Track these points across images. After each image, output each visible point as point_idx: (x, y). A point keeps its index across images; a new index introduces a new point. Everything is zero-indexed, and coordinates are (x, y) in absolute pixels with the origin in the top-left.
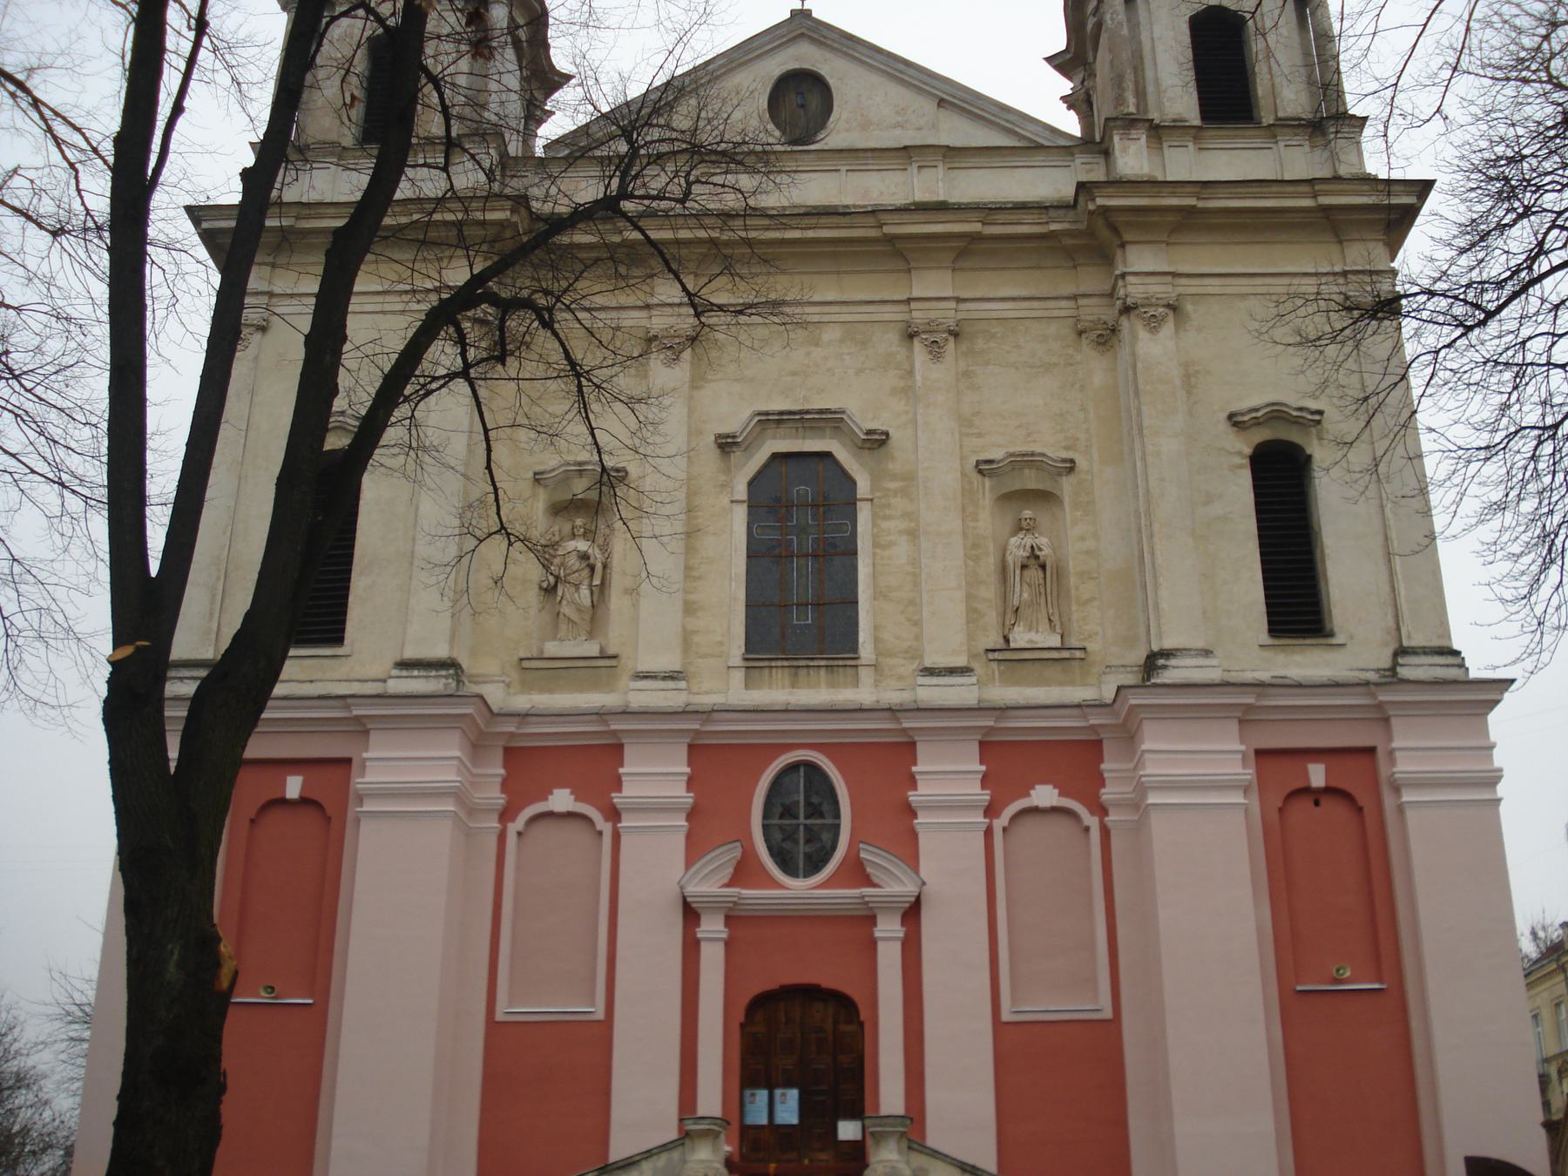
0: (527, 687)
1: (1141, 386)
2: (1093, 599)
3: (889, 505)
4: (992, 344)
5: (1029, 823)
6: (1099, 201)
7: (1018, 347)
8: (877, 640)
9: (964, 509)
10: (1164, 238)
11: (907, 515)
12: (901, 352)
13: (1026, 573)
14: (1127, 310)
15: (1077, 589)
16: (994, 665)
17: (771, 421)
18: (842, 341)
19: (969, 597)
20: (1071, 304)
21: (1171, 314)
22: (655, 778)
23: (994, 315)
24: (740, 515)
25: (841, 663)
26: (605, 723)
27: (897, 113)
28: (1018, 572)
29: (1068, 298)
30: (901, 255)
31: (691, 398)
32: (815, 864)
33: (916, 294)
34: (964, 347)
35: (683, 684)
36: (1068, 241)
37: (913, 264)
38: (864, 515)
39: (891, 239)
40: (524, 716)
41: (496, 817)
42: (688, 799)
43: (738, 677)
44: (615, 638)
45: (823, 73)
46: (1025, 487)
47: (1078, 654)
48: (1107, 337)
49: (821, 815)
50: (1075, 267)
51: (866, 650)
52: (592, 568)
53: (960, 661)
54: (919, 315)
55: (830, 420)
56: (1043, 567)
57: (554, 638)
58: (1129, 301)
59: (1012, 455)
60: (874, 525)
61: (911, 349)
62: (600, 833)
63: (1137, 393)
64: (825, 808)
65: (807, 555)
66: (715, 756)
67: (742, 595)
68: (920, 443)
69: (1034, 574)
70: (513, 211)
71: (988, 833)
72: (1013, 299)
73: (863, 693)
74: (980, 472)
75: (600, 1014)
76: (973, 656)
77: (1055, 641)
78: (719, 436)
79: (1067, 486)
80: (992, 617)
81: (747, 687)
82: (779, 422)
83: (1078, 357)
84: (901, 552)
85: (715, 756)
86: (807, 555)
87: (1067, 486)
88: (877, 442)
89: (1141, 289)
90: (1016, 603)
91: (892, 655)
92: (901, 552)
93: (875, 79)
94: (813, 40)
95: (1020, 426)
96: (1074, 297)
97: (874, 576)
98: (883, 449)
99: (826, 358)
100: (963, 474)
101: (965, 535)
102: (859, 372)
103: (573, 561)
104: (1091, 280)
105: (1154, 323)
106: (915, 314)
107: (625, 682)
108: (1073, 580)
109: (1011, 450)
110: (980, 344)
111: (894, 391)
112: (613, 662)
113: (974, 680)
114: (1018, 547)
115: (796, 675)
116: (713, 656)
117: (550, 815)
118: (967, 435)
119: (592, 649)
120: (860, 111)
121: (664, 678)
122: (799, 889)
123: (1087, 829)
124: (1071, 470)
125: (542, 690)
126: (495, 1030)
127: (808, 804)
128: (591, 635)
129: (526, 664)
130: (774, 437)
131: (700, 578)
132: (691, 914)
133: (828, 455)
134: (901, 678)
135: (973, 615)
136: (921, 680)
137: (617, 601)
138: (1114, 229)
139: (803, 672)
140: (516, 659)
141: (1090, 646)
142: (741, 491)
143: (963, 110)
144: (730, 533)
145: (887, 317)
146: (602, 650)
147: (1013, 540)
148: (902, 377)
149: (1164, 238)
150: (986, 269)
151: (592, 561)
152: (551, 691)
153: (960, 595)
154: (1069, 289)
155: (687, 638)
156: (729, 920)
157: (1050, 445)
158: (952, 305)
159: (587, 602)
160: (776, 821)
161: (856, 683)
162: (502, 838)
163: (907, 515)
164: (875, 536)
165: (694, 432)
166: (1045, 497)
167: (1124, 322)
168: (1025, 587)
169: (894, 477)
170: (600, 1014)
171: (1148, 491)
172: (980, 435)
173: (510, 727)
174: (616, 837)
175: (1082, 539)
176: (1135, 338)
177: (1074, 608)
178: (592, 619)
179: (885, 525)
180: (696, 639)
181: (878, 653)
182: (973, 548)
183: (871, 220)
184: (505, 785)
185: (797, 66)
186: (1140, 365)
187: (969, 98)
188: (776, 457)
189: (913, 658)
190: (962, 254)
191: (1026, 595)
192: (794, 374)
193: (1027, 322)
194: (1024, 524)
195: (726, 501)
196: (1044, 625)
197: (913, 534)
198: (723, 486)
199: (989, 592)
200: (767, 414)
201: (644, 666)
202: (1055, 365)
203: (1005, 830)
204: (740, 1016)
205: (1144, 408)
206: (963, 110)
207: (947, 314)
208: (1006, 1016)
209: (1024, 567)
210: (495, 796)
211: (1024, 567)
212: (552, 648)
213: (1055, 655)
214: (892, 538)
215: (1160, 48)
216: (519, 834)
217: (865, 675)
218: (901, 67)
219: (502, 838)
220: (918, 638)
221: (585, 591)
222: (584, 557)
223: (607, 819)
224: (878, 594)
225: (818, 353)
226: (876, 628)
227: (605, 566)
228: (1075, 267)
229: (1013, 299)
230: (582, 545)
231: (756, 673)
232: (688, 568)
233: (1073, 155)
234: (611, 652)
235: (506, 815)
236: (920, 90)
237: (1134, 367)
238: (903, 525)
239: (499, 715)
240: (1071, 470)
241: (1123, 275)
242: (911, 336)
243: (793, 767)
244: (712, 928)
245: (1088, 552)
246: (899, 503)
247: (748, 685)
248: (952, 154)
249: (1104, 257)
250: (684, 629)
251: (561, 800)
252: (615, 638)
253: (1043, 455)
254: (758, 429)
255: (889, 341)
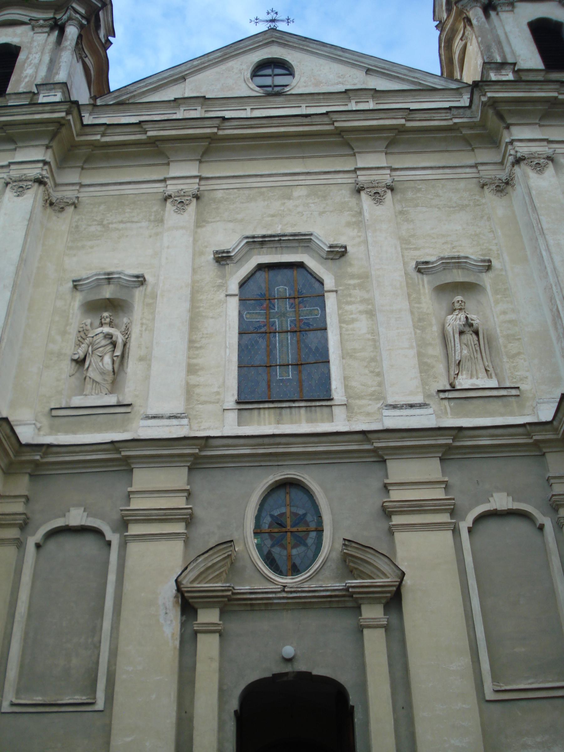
0: (54, 430)
1: (537, 205)
2: (519, 354)
3: (350, 295)
4: (419, 195)
5: (492, 525)
6: (489, 95)
7: (438, 196)
8: (346, 387)
9: (409, 295)
10: (537, 121)
11: (364, 301)
12: (352, 202)
13: (464, 337)
14: (518, 161)
15: (505, 347)
16: (446, 402)
17: (258, 242)
18: (308, 196)
19: (420, 355)
20: (474, 170)
21: (550, 163)
23: (418, 178)
24: (233, 305)
25: (318, 404)
26: (118, 451)
27: (339, 77)
28: (457, 336)
29: (471, 167)
30: (347, 144)
31: (196, 233)
33: (359, 165)
34: (398, 197)
35: (185, 421)
36: (465, 132)
37: (356, 150)
38: (331, 301)
39: (340, 132)
43: (232, 416)
45: (287, 59)
46: (455, 281)
47: (514, 392)
48: (503, 186)
50: (473, 150)
51: (338, 392)
52: (114, 344)
53: (419, 399)
54: (363, 178)
55: (303, 241)
56: (477, 333)
57: (81, 394)
58: (519, 155)
59: (442, 258)
60: (339, 308)
61: (360, 199)
62: (109, 543)
63: (534, 208)
65: (287, 332)
67: (235, 358)
68: (372, 254)
69: (470, 337)
70: (68, 113)
71: (456, 531)
72: (431, 168)
73: (340, 423)
74: (419, 271)
76: (429, 396)
77: (493, 383)
78: (217, 252)
79: (487, 279)
80: (440, 368)
81: (239, 424)
82: (262, 243)
83: (484, 201)
84: (362, 326)
86: (287, 332)
87: (487, 279)
88: (338, 253)
89: (526, 149)
90: (458, 358)
91: (360, 398)
92: (362, 326)
93: (322, 61)
94: (280, 44)
95: (446, 243)
96: (476, 166)
97: (342, 342)
98: (343, 259)
99: (297, 206)
100: (406, 274)
101: (412, 313)
102: (321, 214)
104: (485, 155)
105: (539, 168)
106: (361, 178)
108: (501, 341)
109: (442, 255)
110: (410, 195)
111: (348, 224)
113: (431, 411)
114: (455, 321)
115: (280, 414)
116: (210, 402)
118: (407, 249)
119: (112, 400)
120: (311, 75)
121: (170, 417)
123: (541, 528)
124: (489, 268)
128: (111, 392)
129: (55, 413)
130: (259, 254)
131: (201, 347)
133: (300, 265)
134: (368, 414)
135: (424, 368)
136: (386, 412)
137: (133, 366)
138: (501, 117)
139: (286, 412)
140: (47, 409)
141: (522, 387)
142: (234, 288)
143: (383, 74)
144: (225, 319)
145: (340, 181)
147: (450, 317)
148: (354, 216)
149: (537, 121)
150: (409, 153)
151: (114, 339)
152: (74, 433)
153: (413, 352)
154: (471, 162)
155: (189, 392)
157: (471, 251)
158: (388, 172)
159: (110, 368)
161: (331, 418)
163: (364, 301)
164: (340, 316)
165: (197, 253)
166: (469, 288)
167: (517, 169)
168: (464, 347)
169: (352, 277)
171: (555, 268)
172: (416, 249)
175: (504, 313)
176: (526, 176)
177: (505, 359)
178: (114, 382)
179: (348, 308)
180: (197, 390)
181: (349, 397)
182: (420, 322)
183: (326, 120)
185: (270, 56)
186: (534, 193)
187: (387, 66)
188: (261, 267)
189: (378, 399)
190: (392, 143)
191: (465, 352)
192: (273, 216)
193: (443, 182)
194: (457, 306)
195: (222, 296)
196: (482, 373)
197: (371, 314)
198: (220, 286)
199: (436, 350)
200: (254, 237)
201: (152, 411)
202: (467, 206)
203: (470, 530)
205: (542, 218)
206: (383, 74)
207: (385, 177)
209: (461, 333)
211: (461, 333)
212: (77, 401)
213: (495, 393)
214: (353, 316)
215: (511, 37)
217: (339, 412)
218: (340, 53)
220: (380, 384)
221: (107, 359)
222: (109, 336)
224: (345, 355)
225: (290, 204)
226: (346, 378)
227: (125, 345)
228: (473, 150)
229: (431, 168)
230: (106, 329)
231: (245, 413)
233: (461, 94)
236: (353, 65)
237: (530, 194)
238: (362, 307)
239: (28, 445)
240: (489, 268)
241: (511, 142)
242: (359, 191)
245: (510, 322)
246: (358, 293)
247: (239, 424)
248: (376, 93)
249: (492, 140)
250: (188, 384)
253: (467, 258)
254: (246, 249)
255: (343, 195)
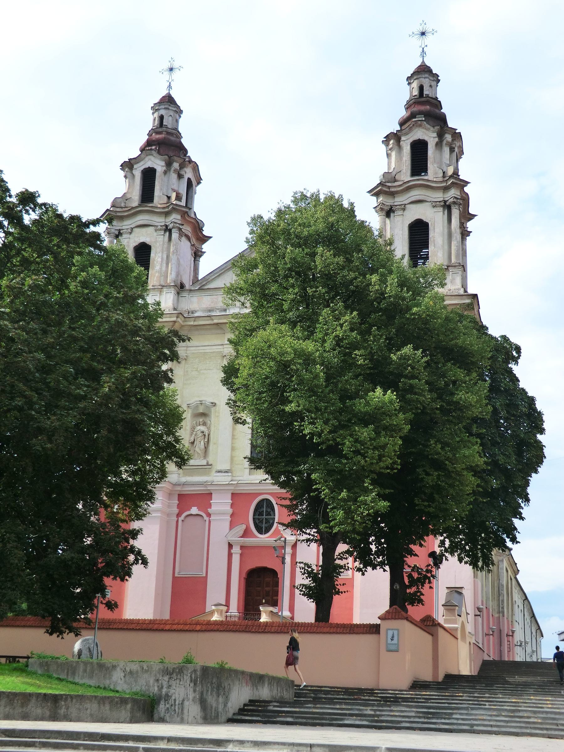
22: (221, 505)
32: (267, 530)
35: (230, 474)
40: (184, 484)
41: (176, 516)
42: (231, 511)
44: (211, 459)
49: (270, 515)
64: (272, 513)
66: (238, 498)
75: (204, 575)
85: (238, 498)
103: (199, 433)
107: (213, 473)
112: (210, 467)
117: (191, 515)
119: (204, 462)
122: (265, 539)
125: (190, 476)
126: (176, 580)
127: (266, 511)
132: (230, 546)
146: (208, 463)
152: (192, 476)
156: (242, 547)
160: (257, 517)
162: (177, 522)
170: (204, 575)
173: (179, 488)
174: (210, 522)
184: (178, 506)
201: (219, 468)
204: (244, 575)
208: (176, 575)
210: (176, 511)
216: (183, 521)
219: (177, 522)
223: (207, 516)
232: (233, 435)
234: (210, 463)
235: (178, 515)
243: (263, 500)
244: (236, 550)
251: (194, 510)
252: (211, 459)
